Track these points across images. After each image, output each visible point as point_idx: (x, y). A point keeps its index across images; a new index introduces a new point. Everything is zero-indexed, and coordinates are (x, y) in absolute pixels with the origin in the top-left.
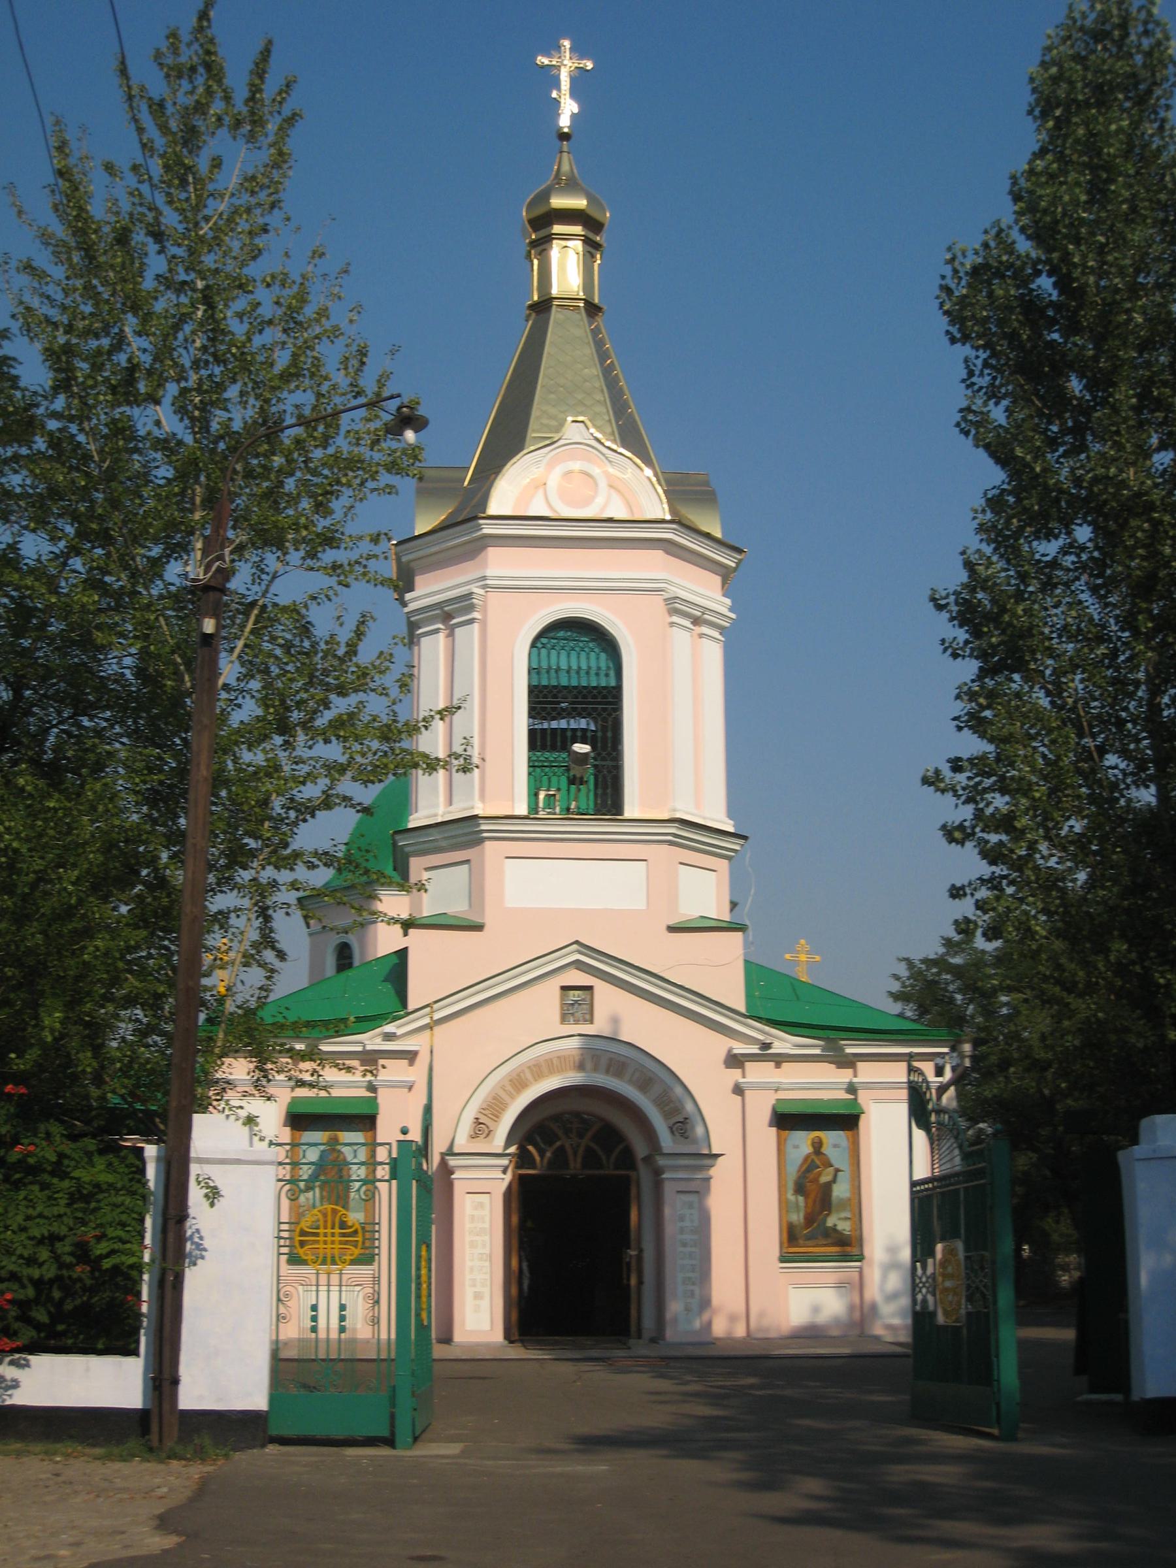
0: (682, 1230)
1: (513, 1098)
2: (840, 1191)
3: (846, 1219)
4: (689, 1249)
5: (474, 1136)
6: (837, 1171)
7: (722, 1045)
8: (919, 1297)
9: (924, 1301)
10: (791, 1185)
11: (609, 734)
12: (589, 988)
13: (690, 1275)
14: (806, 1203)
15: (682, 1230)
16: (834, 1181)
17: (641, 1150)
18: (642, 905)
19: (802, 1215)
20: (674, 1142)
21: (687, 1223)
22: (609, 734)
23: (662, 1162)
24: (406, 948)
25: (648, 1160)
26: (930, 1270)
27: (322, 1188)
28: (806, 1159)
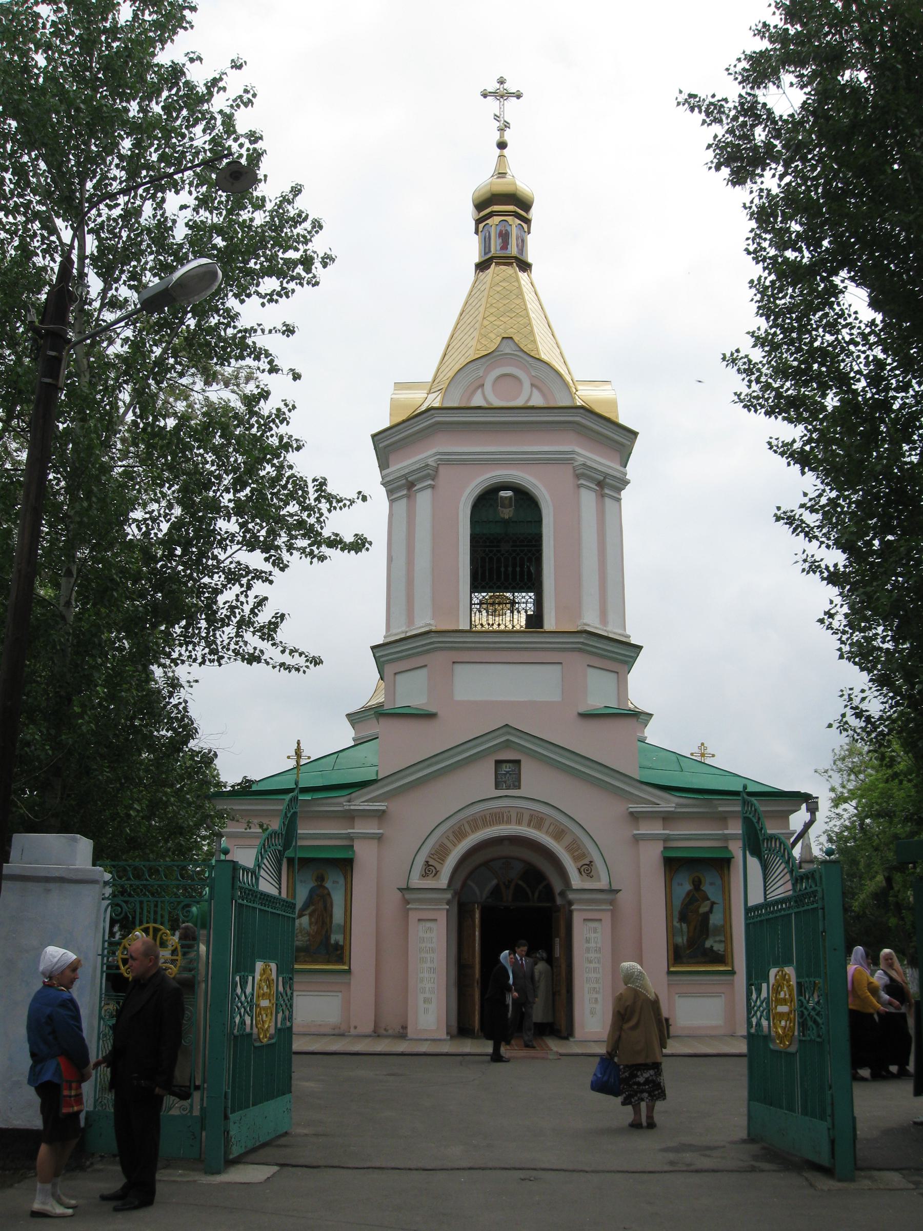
0: (588, 950)
1: (455, 845)
2: (715, 919)
3: (721, 941)
4: (592, 965)
5: (425, 875)
6: (713, 903)
7: (620, 808)
8: (754, 1020)
9: (759, 1024)
10: (676, 914)
11: (518, 569)
12: (517, 762)
13: (595, 985)
14: (688, 928)
15: (588, 950)
16: (711, 911)
17: (558, 887)
18: (560, 699)
19: (685, 938)
20: (582, 881)
21: (592, 945)
22: (518, 569)
23: (571, 896)
24: (652, 715)
25: (562, 894)
26: (764, 994)
27: (311, 915)
28: (688, 894)
